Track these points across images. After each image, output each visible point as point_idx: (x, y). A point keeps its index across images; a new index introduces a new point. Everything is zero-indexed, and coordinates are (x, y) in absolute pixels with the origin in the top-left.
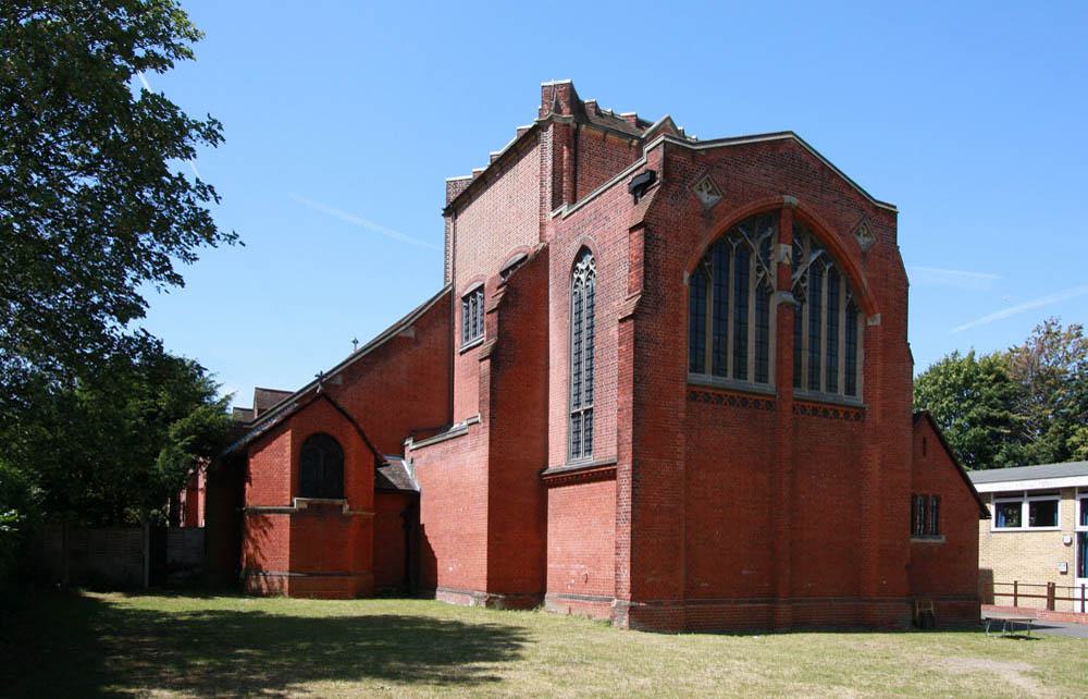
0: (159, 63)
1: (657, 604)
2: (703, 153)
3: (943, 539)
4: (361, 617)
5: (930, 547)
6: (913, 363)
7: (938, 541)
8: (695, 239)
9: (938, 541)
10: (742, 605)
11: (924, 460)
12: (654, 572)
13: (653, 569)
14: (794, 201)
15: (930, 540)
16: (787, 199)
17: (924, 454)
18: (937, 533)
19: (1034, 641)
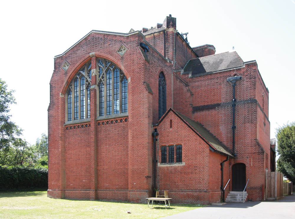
0: (62, 97)
1: (54, 190)
2: (65, 55)
3: (183, 164)
4: (76, 200)
5: (175, 169)
6: (268, 92)
7: (180, 165)
8: (63, 82)
9: (180, 165)
10: (82, 191)
11: (171, 129)
12: (54, 181)
13: (54, 180)
14: (93, 53)
15: (176, 165)
16: (91, 54)
17: (171, 127)
18: (179, 160)
19: (174, 209)
